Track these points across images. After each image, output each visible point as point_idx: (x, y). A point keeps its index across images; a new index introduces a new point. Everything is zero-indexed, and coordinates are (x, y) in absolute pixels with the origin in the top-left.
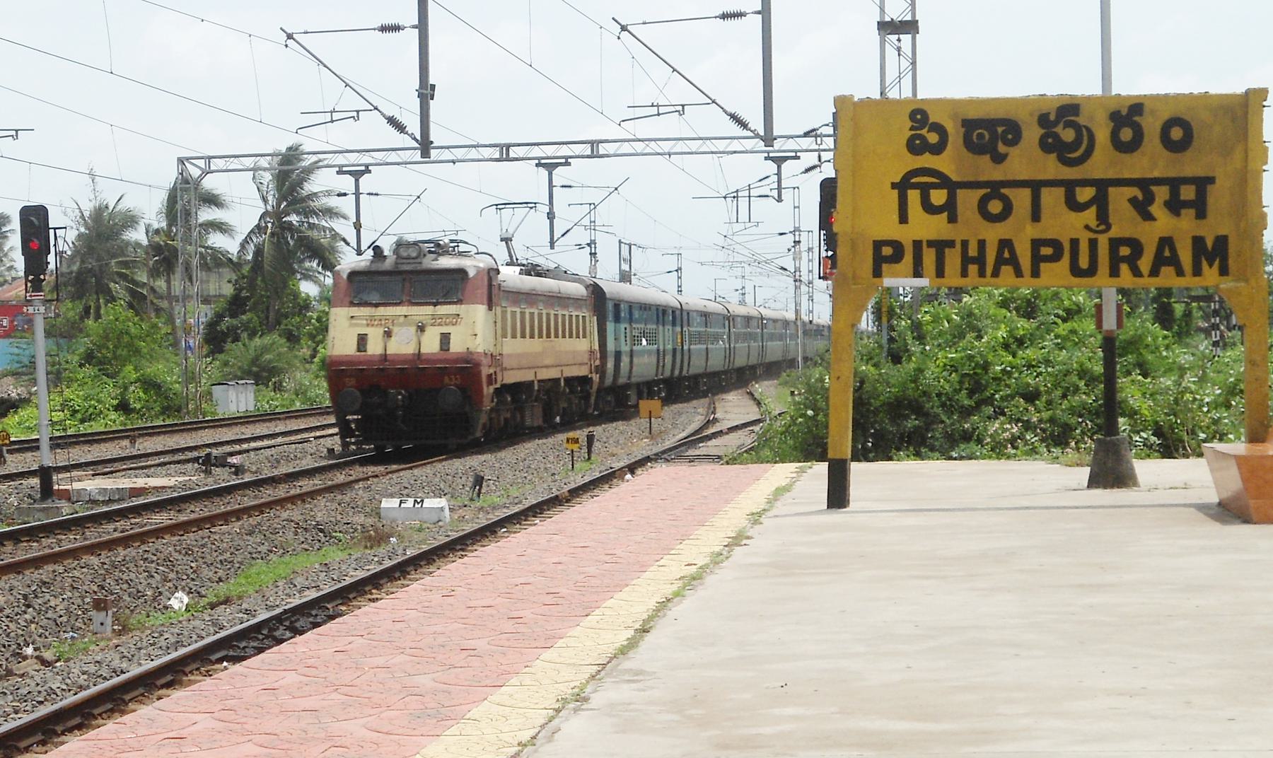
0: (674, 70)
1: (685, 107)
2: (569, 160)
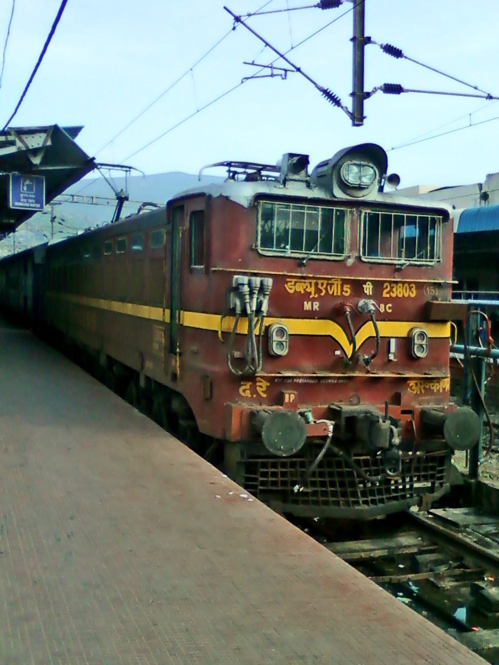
0: (267, 44)
1: (288, 72)
2: (171, 224)
